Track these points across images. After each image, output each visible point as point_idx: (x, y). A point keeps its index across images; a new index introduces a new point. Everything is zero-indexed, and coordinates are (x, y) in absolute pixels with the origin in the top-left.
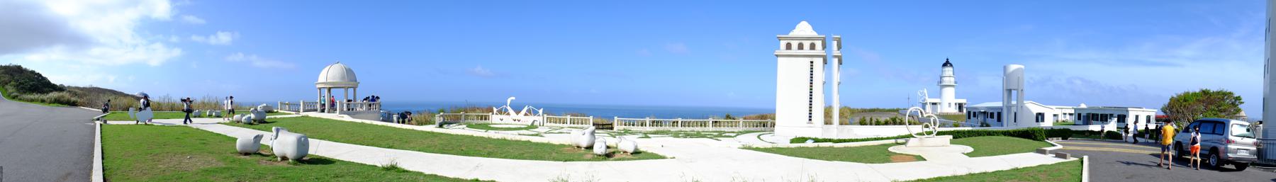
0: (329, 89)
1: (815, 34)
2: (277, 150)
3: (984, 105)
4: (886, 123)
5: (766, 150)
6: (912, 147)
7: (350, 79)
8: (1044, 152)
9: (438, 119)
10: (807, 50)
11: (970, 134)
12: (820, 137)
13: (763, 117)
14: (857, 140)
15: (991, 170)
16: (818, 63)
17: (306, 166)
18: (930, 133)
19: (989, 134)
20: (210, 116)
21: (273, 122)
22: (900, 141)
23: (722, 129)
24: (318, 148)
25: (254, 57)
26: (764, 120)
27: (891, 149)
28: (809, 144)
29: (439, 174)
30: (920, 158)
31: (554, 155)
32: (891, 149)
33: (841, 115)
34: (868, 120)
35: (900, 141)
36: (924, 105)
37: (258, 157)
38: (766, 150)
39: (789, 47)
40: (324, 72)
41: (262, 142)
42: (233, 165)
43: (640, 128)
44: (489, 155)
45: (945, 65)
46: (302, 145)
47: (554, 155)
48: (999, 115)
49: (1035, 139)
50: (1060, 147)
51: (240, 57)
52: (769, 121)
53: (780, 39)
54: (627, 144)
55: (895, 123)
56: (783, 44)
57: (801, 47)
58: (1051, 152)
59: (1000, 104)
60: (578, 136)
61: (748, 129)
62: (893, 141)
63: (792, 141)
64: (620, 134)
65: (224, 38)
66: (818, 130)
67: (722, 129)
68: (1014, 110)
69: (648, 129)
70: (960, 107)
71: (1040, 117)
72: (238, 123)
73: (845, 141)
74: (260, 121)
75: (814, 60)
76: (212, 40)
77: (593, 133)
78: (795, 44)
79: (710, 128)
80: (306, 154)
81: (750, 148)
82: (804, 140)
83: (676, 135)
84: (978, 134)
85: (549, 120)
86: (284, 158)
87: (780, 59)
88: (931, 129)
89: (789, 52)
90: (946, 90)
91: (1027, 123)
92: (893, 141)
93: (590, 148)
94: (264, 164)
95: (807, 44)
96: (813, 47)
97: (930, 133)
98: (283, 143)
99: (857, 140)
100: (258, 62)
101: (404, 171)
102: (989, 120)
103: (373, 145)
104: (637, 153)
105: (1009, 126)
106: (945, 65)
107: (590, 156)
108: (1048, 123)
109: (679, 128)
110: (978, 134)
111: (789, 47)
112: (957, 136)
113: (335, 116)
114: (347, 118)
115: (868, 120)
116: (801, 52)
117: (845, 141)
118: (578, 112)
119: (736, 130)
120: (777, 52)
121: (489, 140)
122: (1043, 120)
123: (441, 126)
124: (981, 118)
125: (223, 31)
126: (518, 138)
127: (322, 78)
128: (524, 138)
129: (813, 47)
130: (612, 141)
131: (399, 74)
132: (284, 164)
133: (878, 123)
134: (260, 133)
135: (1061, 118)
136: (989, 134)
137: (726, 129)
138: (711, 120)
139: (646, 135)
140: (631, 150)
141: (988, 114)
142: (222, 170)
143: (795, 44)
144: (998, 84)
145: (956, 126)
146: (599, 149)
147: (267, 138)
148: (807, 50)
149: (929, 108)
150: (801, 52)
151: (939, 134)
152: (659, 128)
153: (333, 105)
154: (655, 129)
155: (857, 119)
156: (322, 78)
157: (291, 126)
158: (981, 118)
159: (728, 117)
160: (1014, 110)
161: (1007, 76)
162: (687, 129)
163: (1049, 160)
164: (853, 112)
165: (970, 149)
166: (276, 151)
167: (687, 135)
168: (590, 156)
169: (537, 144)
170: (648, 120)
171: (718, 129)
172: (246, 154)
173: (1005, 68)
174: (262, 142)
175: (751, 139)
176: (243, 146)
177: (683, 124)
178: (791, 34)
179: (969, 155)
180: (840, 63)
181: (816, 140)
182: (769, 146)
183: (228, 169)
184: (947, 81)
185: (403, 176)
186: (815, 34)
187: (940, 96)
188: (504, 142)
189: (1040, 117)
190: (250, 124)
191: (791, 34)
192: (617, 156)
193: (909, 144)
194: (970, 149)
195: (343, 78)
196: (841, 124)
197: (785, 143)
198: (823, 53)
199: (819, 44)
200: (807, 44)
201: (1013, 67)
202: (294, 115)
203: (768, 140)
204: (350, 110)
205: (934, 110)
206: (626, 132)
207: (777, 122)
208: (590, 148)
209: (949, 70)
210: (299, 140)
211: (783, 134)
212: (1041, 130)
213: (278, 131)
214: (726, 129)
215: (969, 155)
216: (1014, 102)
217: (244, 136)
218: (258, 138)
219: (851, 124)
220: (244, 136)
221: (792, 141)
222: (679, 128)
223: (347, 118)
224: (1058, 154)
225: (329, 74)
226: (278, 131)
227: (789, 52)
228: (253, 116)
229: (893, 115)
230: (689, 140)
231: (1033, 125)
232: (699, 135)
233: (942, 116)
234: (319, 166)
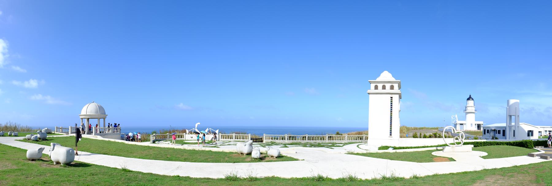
0: (88, 119)
1: (393, 79)
2: (54, 158)
3: (493, 126)
4: (430, 137)
5: (363, 155)
6: (447, 152)
7: (101, 113)
8: (532, 156)
9: (152, 138)
10: (388, 90)
11: (485, 144)
12: (397, 146)
13: (359, 133)
14: (411, 148)
15: (499, 167)
16: (396, 98)
17: (73, 168)
18: (459, 143)
19: (498, 144)
20: (10, 135)
21: (51, 140)
22: (439, 148)
23: (334, 141)
24: (82, 157)
25: (49, 97)
26: (361, 136)
27: (433, 153)
28: (390, 150)
29: (154, 173)
30: (452, 160)
31: (226, 159)
32: (433, 153)
33: (401, 131)
34: (418, 135)
35: (439, 148)
36: (455, 125)
37: (41, 162)
38: (363, 155)
39: (376, 87)
40: (85, 108)
41: (44, 152)
42: (25, 168)
43: (281, 141)
44: (185, 160)
45: (468, 99)
46: (70, 155)
47: (226, 159)
48: (504, 131)
49: (527, 147)
50: (543, 152)
51: (39, 97)
52: (364, 136)
53: (370, 83)
54: (273, 151)
55: (436, 137)
56: (373, 86)
57: (384, 87)
58: (537, 155)
59: (504, 125)
60: (242, 147)
61: (350, 141)
62: (435, 148)
63: (380, 149)
64: (268, 145)
65: (33, 83)
66: (396, 141)
67: (334, 141)
68: (513, 129)
69: (287, 141)
70: (479, 126)
71: (530, 133)
72: (28, 140)
73: (404, 148)
74: (43, 139)
75: (393, 96)
76: (26, 85)
77: (251, 145)
78: (380, 86)
79: (327, 141)
80: (73, 161)
81: (352, 154)
82: (387, 148)
83: (305, 145)
84: (491, 144)
85: (223, 137)
86: (58, 163)
87: (370, 95)
88: (460, 141)
89: (376, 91)
90: (468, 115)
91: (521, 137)
92: (435, 148)
93: (249, 154)
94: (44, 166)
95: (388, 86)
96: (392, 88)
97: (459, 143)
98: (58, 153)
99: (411, 148)
100: (50, 100)
101: (130, 171)
102: (497, 135)
103: (115, 155)
104: (280, 157)
105: (510, 138)
106: (468, 99)
107: (249, 159)
108: (535, 137)
109: (307, 141)
110: (491, 144)
111: (376, 87)
112: (476, 145)
113: (92, 137)
114: (99, 138)
115: (418, 135)
116: (384, 91)
117: (404, 148)
118: (240, 133)
119: (343, 142)
120: (369, 91)
121: (185, 151)
122: (532, 135)
123: (154, 142)
124: (492, 134)
125: (33, 79)
126: (204, 149)
127: (83, 112)
128: (207, 149)
129: (392, 88)
130: (263, 150)
131: (135, 108)
132: (58, 167)
133: (425, 137)
134: (42, 146)
135: (544, 134)
136: (498, 144)
137: (337, 141)
138: (327, 136)
139: (285, 146)
140: (276, 154)
141: (497, 131)
142: (14, 171)
143: (380, 86)
144: (503, 112)
145: (476, 139)
146: (255, 154)
147: (47, 150)
148: (388, 90)
149: (458, 127)
150: (384, 91)
151: (465, 144)
152: (294, 141)
153: (90, 128)
154: (291, 141)
155: (411, 134)
156: (83, 112)
157: (63, 142)
158: (492, 134)
159: (338, 134)
160: (513, 129)
161: (509, 107)
162: (312, 141)
163: (537, 160)
164: (408, 129)
165: (485, 154)
166: (53, 158)
167: (311, 145)
168: (249, 159)
169: (216, 153)
170: (286, 136)
171: (332, 141)
172: (33, 160)
173: (508, 102)
174: (44, 152)
175: (353, 147)
176: (31, 155)
177: (309, 138)
178: (378, 79)
179: (484, 157)
180: (400, 98)
181: (395, 148)
182: (365, 152)
183: (20, 170)
184: (469, 109)
185: (289, 182)
186: (393, 79)
187: (465, 119)
188: (194, 152)
189: (530, 133)
190: (36, 141)
191: (378, 79)
192: (267, 159)
193: (445, 150)
194: (485, 154)
195: (97, 112)
196: (401, 137)
197: (375, 150)
198: (399, 92)
199: (396, 86)
200: (388, 86)
201: (512, 101)
202: (65, 135)
203: (364, 148)
204: (101, 133)
205: (461, 129)
206: (273, 144)
207: (369, 136)
208: (249, 154)
209: (471, 103)
210: (68, 152)
211: (373, 144)
212: (530, 142)
213: (54, 145)
214: (337, 141)
215: (484, 157)
216: (513, 124)
217: (32, 149)
218: (41, 150)
219: (407, 137)
220: (32, 149)
221: (380, 149)
222: (307, 141)
223: (99, 138)
224: (542, 157)
225: (88, 109)
226: (54, 145)
227: (376, 91)
228: (38, 136)
229: (435, 131)
230: (313, 148)
231: (526, 138)
232: (319, 145)
233: (466, 132)
234: (81, 168)
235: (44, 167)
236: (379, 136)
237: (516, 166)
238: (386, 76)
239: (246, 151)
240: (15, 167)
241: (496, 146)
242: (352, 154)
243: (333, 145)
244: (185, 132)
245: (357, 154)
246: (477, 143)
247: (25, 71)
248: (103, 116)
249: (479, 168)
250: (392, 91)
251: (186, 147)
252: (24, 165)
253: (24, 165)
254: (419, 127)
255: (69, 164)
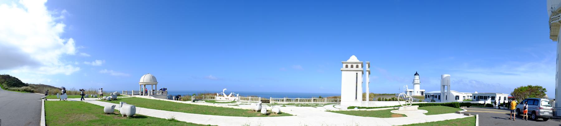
0: (145, 85)
1: (358, 61)
2: (122, 112)
3: (432, 92)
4: (390, 100)
5: (337, 112)
6: (401, 111)
7: (154, 81)
8: (459, 113)
9: (193, 98)
10: (355, 68)
11: (426, 105)
12: (361, 106)
13: (335, 97)
14: (377, 108)
16: (360, 74)
17: (135, 119)
18: (409, 104)
19: (435, 105)
20: (92, 97)
21: (120, 100)
23: (318, 103)
24: (140, 111)
26: (336, 99)
27: (392, 112)
28: (356, 109)
29: (193, 122)
30: (405, 116)
32: (392, 112)
33: (370, 97)
34: (382, 99)
36: (406, 92)
37: (113, 115)
38: (337, 112)
39: (347, 66)
41: (115, 108)
42: (103, 119)
43: (281, 102)
44: (215, 114)
45: (415, 75)
46: (133, 110)
47: (244, 114)
48: (439, 96)
49: (455, 107)
50: (466, 111)
51: (106, 71)
52: (338, 99)
53: (343, 63)
54: (276, 109)
55: (393, 100)
56: (344, 65)
57: (352, 67)
58: (462, 113)
59: (439, 92)
60: (254, 106)
61: (329, 103)
62: (393, 108)
63: (348, 108)
64: (273, 105)
65: (99, 63)
66: (367, 104)
67: (318, 103)
68: (446, 94)
69: (285, 103)
70: (422, 93)
71: (457, 97)
72: (105, 100)
73: (371, 108)
74: (114, 99)
75: (358, 72)
76: (93, 64)
77: (261, 105)
78: (349, 65)
81: (330, 111)
82: (353, 107)
83: (297, 105)
84: (430, 105)
85: (242, 99)
86: (125, 116)
89: (347, 69)
91: (452, 100)
92: (393, 108)
93: (259, 111)
94: (116, 118)
95: (355, 65)
96: (357, 67)
97: (409, 104)
98: (124, 109)
99: (377, 108)
100: (113, 73)
101: (178, 121)
102: (435, 99)
103: (164, 110)
104: (280, 113)
105: (443, 101)
106: (415, 75)
107: (259, 115)
108: (461, 100)
109: (299, 102)
110: (430, 105)
111: (347, 66)
112: (421, 106)
113: (147, 97)
114: (152, 98)
115: (382, 99)
116: (352, 69)
117: (371, 108)
118: (254, 95)
119: (324, 103)
120: (342, 69)
121: (215, 108)
122: (458, 99)
123: (194, 101)
124: (431, 98)
126: (228, 107)
127: (141, 81)
128: (231, 107)
129: (357, 67)
130: (269, 108)
131: (176, 78)
132: (125, 118)
133: (386, 100)
134: (114, 104)
135: (466, 98)
136: (435, 105)
137: (319, 103)
138: (312, 99)
139: (284, 105)
140: (277, 112)
141: (434, 96)
142: (97, 121)
143: (349, 65)
144: (438, 83)
146: (263, 111)
147: (118, 107)
148: (355, 68)
149: (408, 93)
150: (352, 69)
151: (413, 105)
153: (146, 92)
154: (288, 103)
155: (377, 98)
157: (128, 101)
158: (431, 98)
159: (320, 97)
160: (446, 94)
161: (443, 79)
162: (302, 103)
163: (461, 116)
164: (375, 95)
165: (427, 112)
166: (121, 113)
167: (302, 105)
168: (259, 115)
169: (236, 109)
170: (285, 99)
171: (316, 103)
172: (108, 114)
173: (442, 76)
174: (115, 108)
175: (330, 107)
176: (107, 110)
177: (300, 101)
178: (348, 61)
179: (426, 114)
180: (369, 73)
181: (359, 108)
182: (338, 110)
183: (100, 120)
184: (416, 81)
186: (358, 61)
187: (413, 88)
189: (457, 97)
190: (110, 100)
191: (348, 61)
192: (271, 114)
194: (427, 112)
195: (151, 80)
196: (370, 100)
197: (345, 109)
198: (362, 69)
199: (360, 65)
200: (355, 65)
201: (445, 76)
202: (129, 96)
203: (338, 107)
204: (154, 95)
206: (275, 104)
207: (342, 99)
208: (259, 111)
209: (417, 77)
210: (131, 108)
211: (344, 105)
212: (457, 103)
213: (122, 103)
214: (319, 103)
215: (426, 114)
216: (446, 91)
217: (107, 106)
218: (113, 107)
219: (374, 100)
220: (107, 106)
221: (348, 108)
222: (299, 102)
223: (152, 98)
224: (465, 114)
225: (145, 79)
226: (122, 103)
227: (347, 69)
228: (111, 97)
229: (393, 97)
230: (303, 107)
231: (454, 101)
232: (307, 105)
233: (414, 97)
235: (116, 119)
236: (348, 99)
237: (447, 120)
238: (353, 59)
239: (257, 109)
240: (98, 118)
241: (434, 107)
242: (330, 111)
243: (317, 105)
244: (216, 95)
245: (333, 112)
246: (421, 104)
247: (88, 55)
248: (155, 83)
249: (423, 121)
250: (357, 69)
251: (216, 105)
252: (103, 117)
253: (103, 117)
254: (382, 93)
255: (132, 116)
